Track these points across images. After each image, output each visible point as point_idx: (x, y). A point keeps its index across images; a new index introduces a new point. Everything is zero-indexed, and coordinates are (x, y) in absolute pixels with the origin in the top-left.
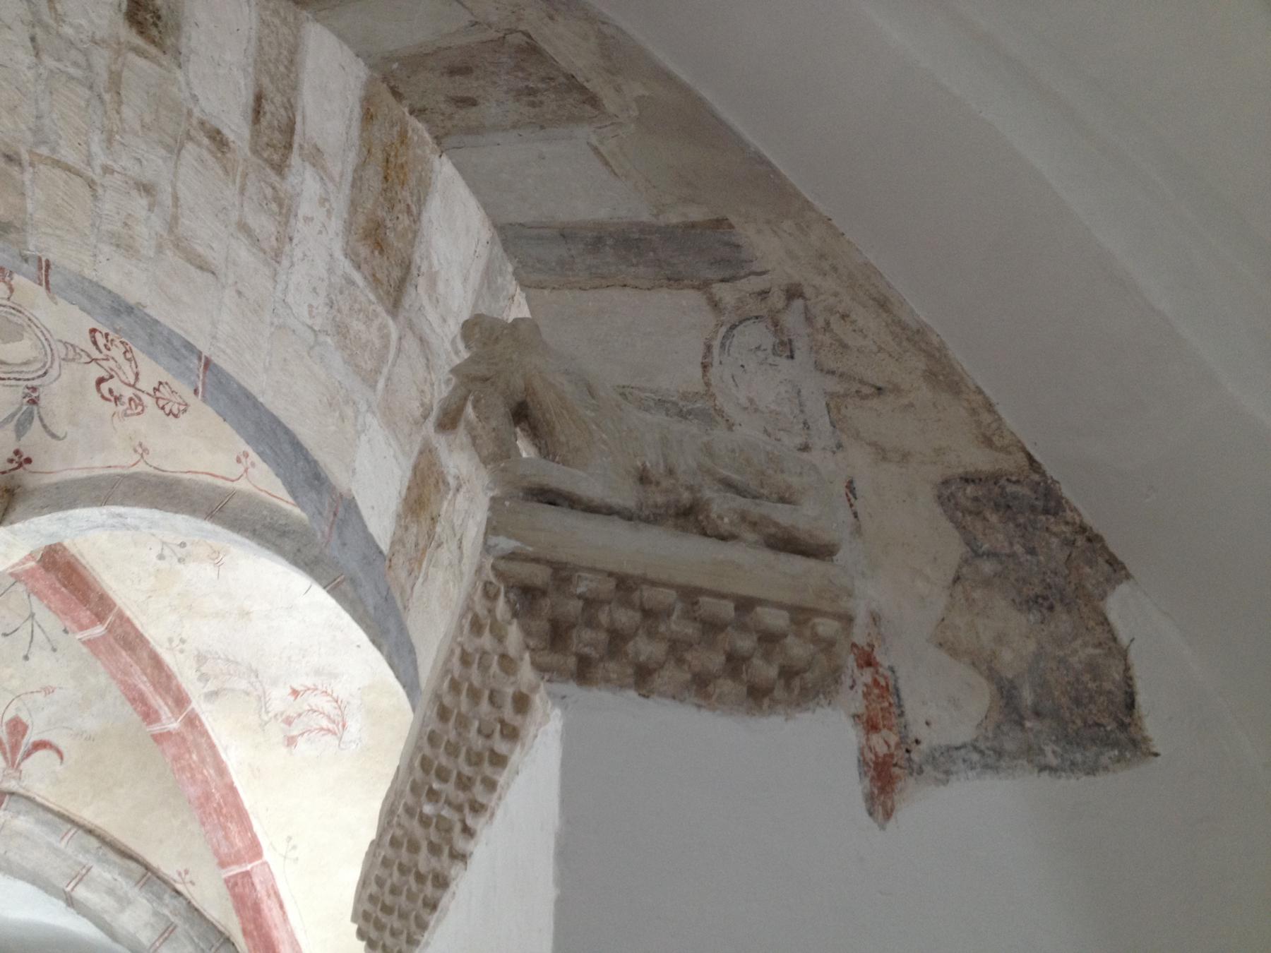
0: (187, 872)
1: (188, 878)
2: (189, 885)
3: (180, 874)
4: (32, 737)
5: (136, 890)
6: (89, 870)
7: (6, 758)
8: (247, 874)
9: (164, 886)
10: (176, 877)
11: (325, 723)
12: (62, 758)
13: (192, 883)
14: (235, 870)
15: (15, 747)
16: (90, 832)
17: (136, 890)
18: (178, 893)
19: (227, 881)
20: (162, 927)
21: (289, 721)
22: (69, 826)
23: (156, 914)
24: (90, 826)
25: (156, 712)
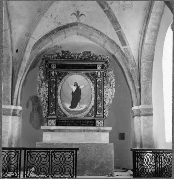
4: (80, 14)
7: (77, 17)
8: (120, 31)
11: (129, 6)
12: (85, 16)
14: (118, 31)
15: (78, 15)
18: (106, 36)
19: (117, 33)
21: (123, 6)
25: (104, 7)
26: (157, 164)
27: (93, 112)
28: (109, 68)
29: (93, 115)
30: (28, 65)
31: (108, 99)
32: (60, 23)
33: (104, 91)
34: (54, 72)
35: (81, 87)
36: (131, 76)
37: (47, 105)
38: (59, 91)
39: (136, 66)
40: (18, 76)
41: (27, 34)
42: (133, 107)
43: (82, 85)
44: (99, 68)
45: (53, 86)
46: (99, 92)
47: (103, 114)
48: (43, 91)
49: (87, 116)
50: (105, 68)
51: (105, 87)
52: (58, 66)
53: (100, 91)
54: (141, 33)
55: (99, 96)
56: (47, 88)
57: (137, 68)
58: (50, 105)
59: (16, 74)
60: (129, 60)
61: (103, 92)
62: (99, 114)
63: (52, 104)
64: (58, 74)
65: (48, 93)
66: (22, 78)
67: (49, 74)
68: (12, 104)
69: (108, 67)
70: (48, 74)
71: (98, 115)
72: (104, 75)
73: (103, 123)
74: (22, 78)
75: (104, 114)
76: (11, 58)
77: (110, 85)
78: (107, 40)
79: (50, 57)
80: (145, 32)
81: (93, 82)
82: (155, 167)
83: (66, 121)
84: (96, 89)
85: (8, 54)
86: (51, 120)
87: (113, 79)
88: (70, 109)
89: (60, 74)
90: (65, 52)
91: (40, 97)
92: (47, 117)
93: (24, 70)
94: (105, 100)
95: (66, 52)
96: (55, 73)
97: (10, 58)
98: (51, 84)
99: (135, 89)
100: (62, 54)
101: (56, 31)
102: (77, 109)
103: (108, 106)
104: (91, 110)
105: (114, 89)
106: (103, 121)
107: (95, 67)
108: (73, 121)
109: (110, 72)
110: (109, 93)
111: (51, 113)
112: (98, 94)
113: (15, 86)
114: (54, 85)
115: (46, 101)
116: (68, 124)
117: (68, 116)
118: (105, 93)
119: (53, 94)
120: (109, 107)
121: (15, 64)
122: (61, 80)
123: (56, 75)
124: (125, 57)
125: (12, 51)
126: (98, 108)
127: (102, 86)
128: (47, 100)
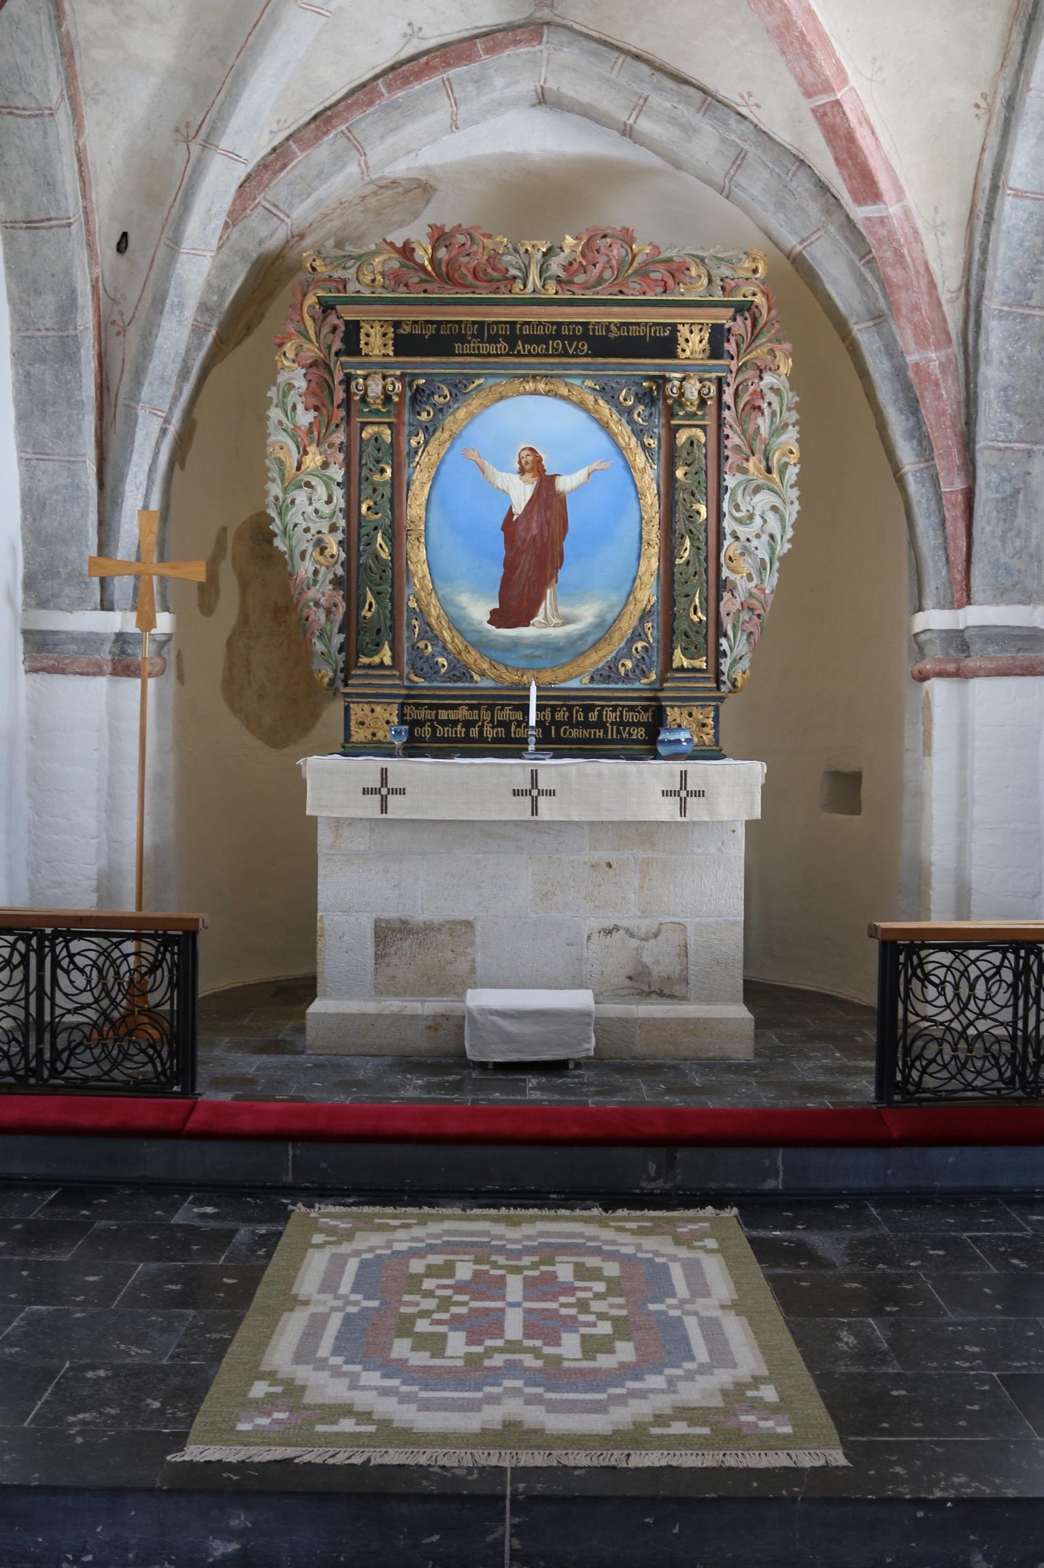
0: (750, 95)
1: (752, 101)
2: (754, 109)
3: (742, 97)
5: (699, 116)
6: (646, 100)
9: (727, 110)
10: (738, 100)
13: (758, 106)
14: (824, 99)
16: (637, 57)
17: (699, 116)
19: (814, 111)
20: (732, 153)
22: (616, 54)
23: (723, 140)
24: (675, 72)
26: (1027, 1009)
27: (645, 648)
28: (759, 353)
29: (644, 674)
30: (198, 331)
31: (746, 565)
32: (413, 31)
33: (726, 506)
34: (381, 383)
35: (564, 484)
36: (913, 406)
37: (342, 609)
38: (415, 509)
39: (950, 340)
40: (141, 413)
41: (188, 125)
42: (920, 616)
43: (571, 470)
44: (693, 344)
45: (377, 478)
46: (692, 516)
47: (712, 668)
48: (310, 509)
49: (608, 679)
50: (730, 347)
51: (730, 481)
52: (407, 343)
53: (696, 506)
54: (990, 110)
55: (688, 543)
56: (338, 493)
57: (956, 349)
58: (360, 607)
59: (121, 402)
60: (903, 297)
61: (720, 515)
62: (686, 663)
63: (370, 598)
64: (409, 394)
65: (342, 523)
66: (167, 421)
67: (348, 391)
68: (106, 605)
69: (755, 336)
70: (340, 394)
71: (682, 669)
72: (728, 398)
73: (716, 727)
74: (167, 421)
75: (718, 664)
76: (85, 300)
77: (769, 471)
78: (752, 151)
79: (350, 274)
80: (1011, 105)
81: (645, 448)
82: (1010, 1029)
83: (463, 714)
84: (669, 485)
85: (67, 272)
86: (367, 708)
87: (786, 426)
88: (492, 628)
89: (418, 398)
90: (451, 235)
91: (291, 556)
92: (339, 684)
93: (173, 369)
94: (733, 571)
95: (461, 239)
96: (384, 387)
97: (80, 301)
98: (361, 466)
99: (939, 497)
100: (434, 249)
101: (390, 88)
102: (542, 628)
103: (751, 609)
104: (632, 641)
105: (793, 494)
106: (717, 709)
107: (665, 345)
108: (520, 41)
109: (768, 378)
110: (758, 521)
111: (364, 660)
112: (680, 527)
113: (121, 478)
114: (383, 471)
115: (331, 576)
116: (481, 732)
117: (476, 677)
118: (727, 524)
119: (376, 528)
120: (759, 616)
121: (114, 329)
122: (429, 430)
123: (396, 399)
124: (872, 271)
125: (90, 246)
126: (681, 625)
127: (712, 472)
128: (340, 571)
